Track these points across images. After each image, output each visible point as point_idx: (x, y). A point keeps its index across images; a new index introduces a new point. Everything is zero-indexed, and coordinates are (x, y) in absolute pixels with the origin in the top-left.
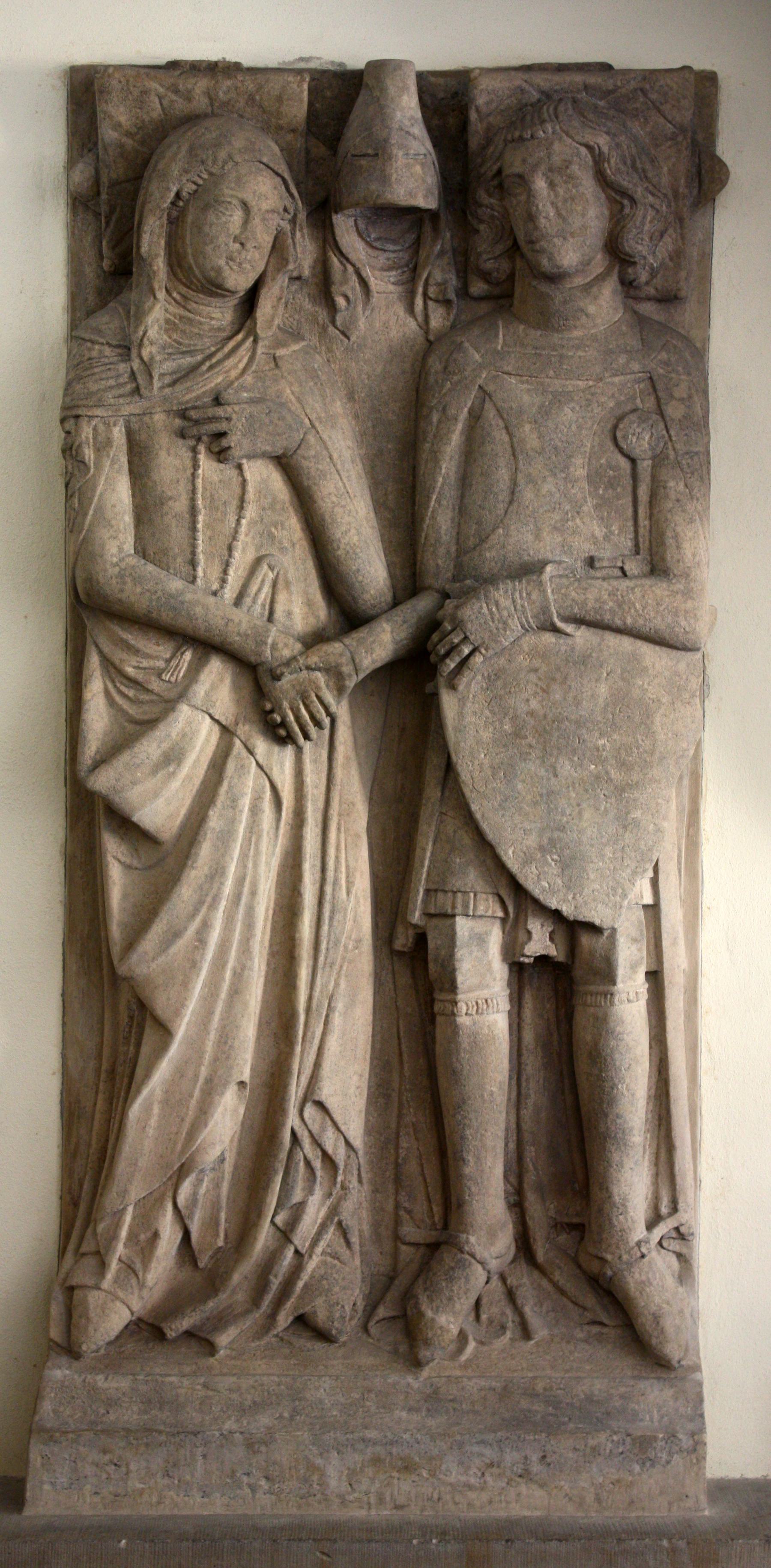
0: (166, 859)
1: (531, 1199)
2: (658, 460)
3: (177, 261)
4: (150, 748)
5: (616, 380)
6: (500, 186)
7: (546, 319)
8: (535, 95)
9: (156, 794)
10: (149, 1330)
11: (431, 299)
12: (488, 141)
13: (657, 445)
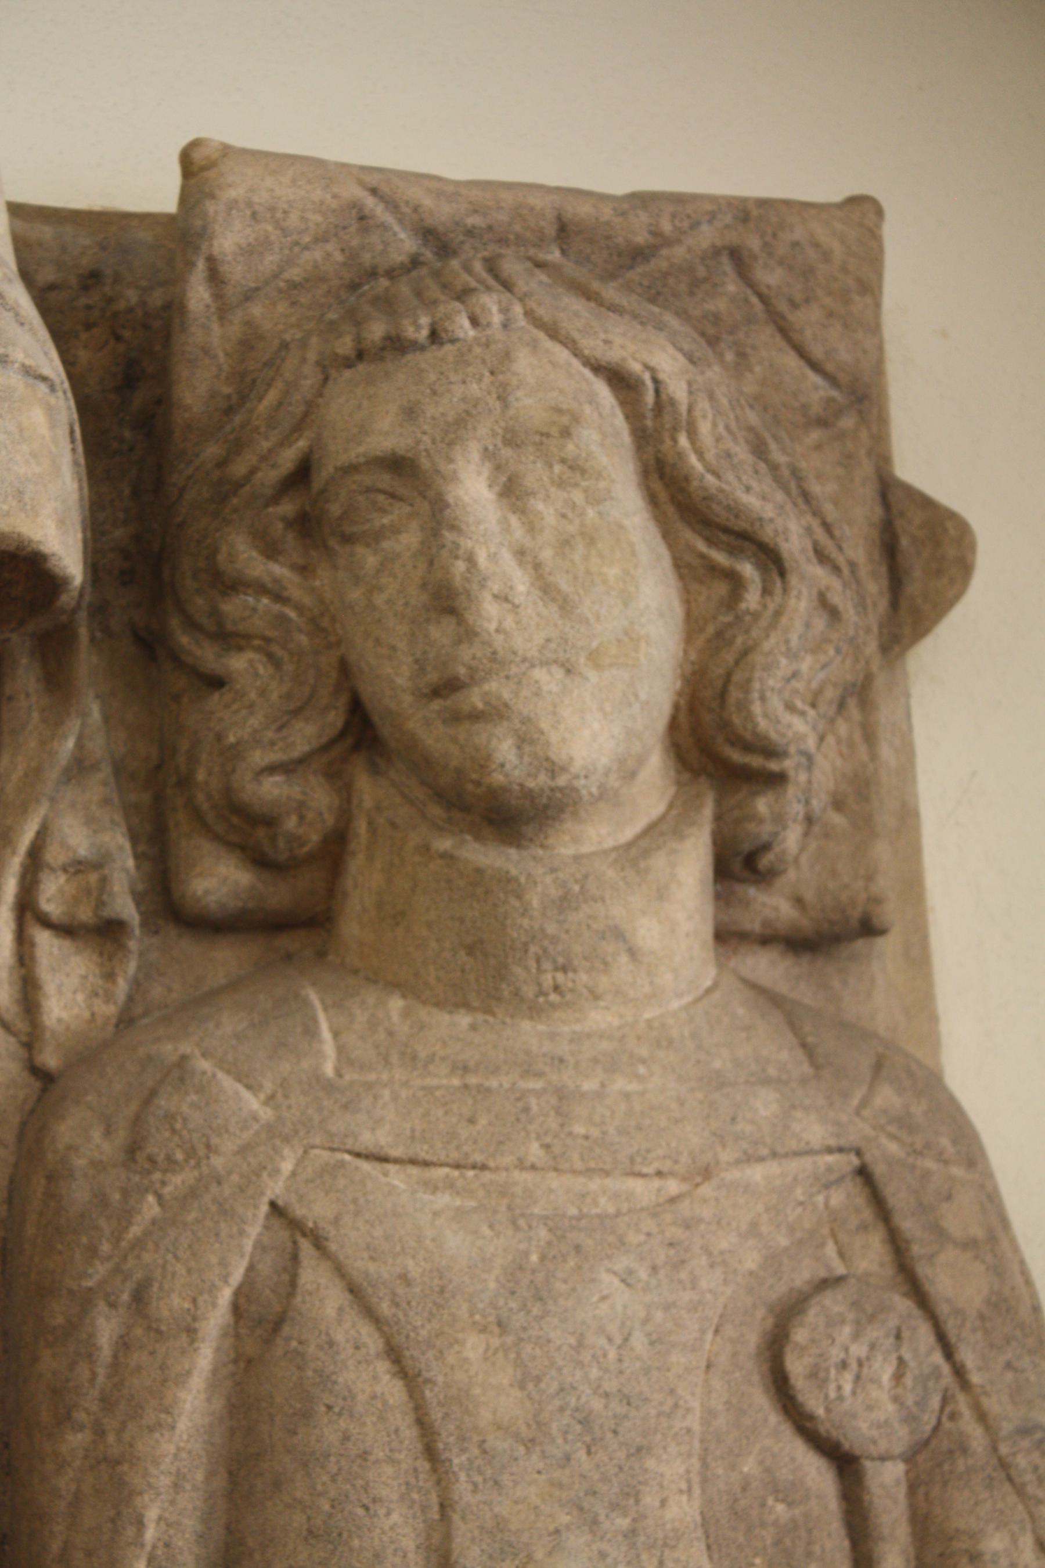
2: (931, 1460)
5: (757, 1174)
6: (308, 526)
7: (488, 967)
8: (405, 243)
11: (46, 922)
12: (245, 387)
13: (921, 1403)
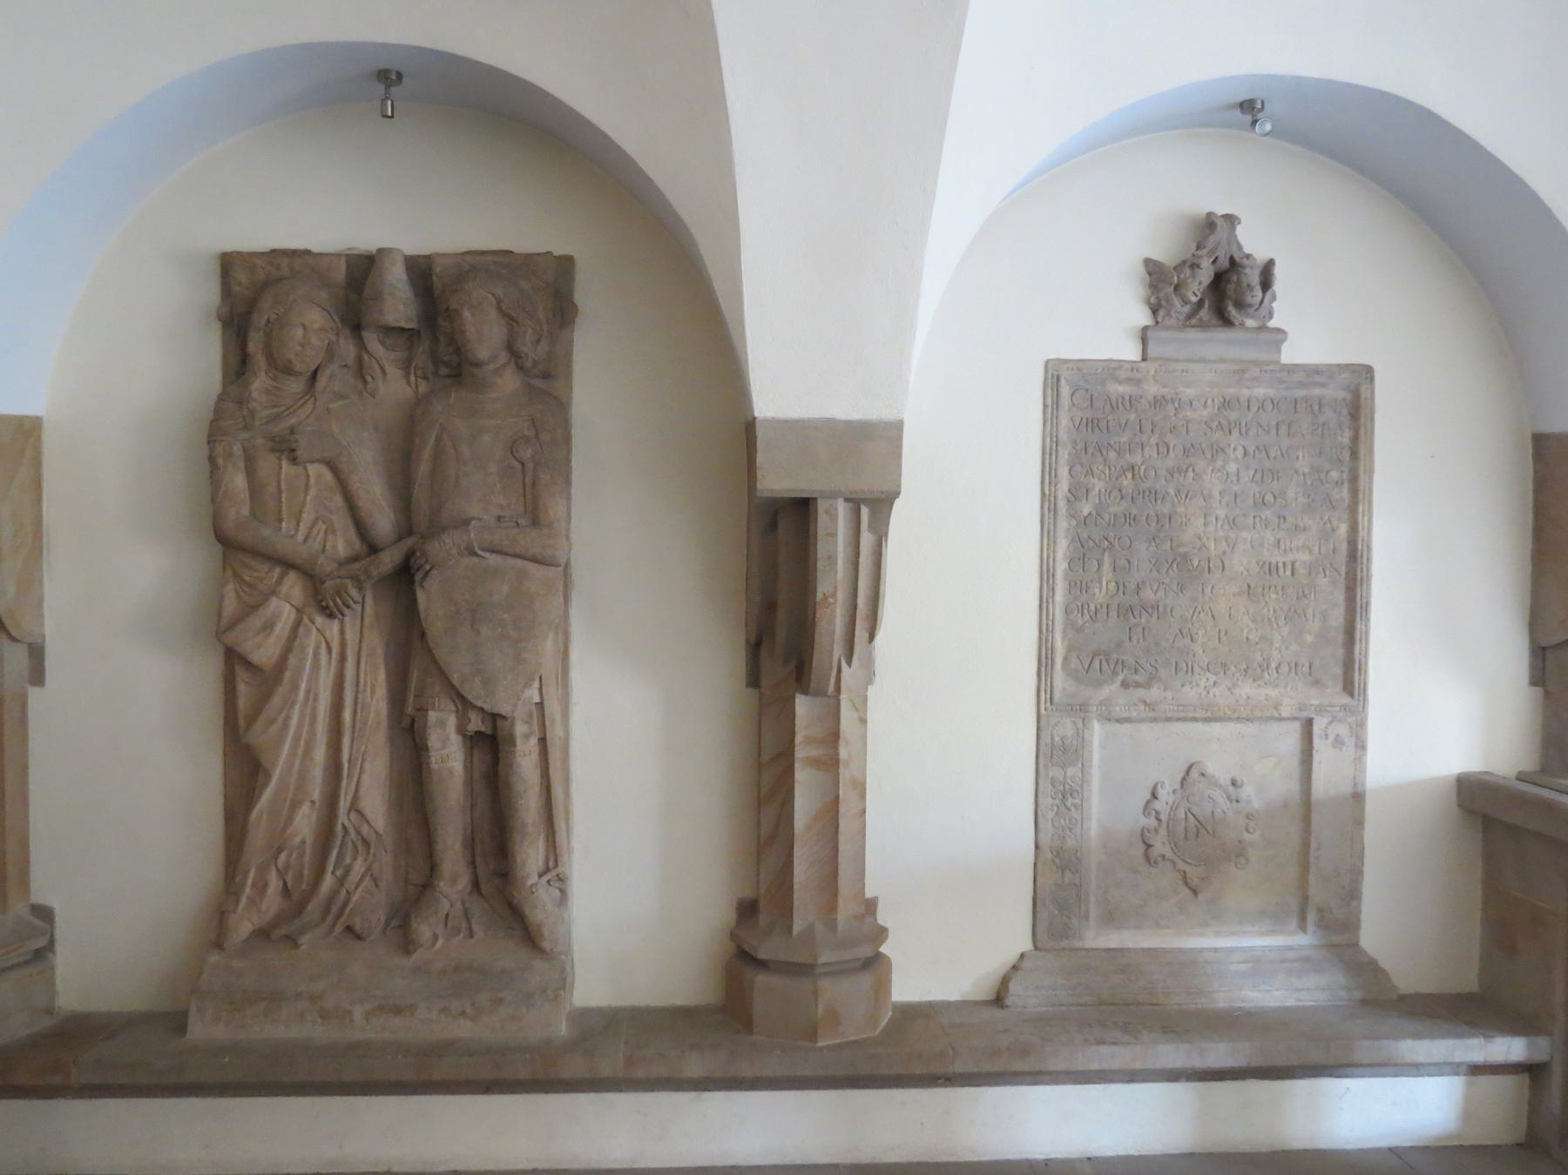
0: (270, 679)
1: (479, 860)
3: (270, 358)
4: (255, 621)
9: (259, 646)
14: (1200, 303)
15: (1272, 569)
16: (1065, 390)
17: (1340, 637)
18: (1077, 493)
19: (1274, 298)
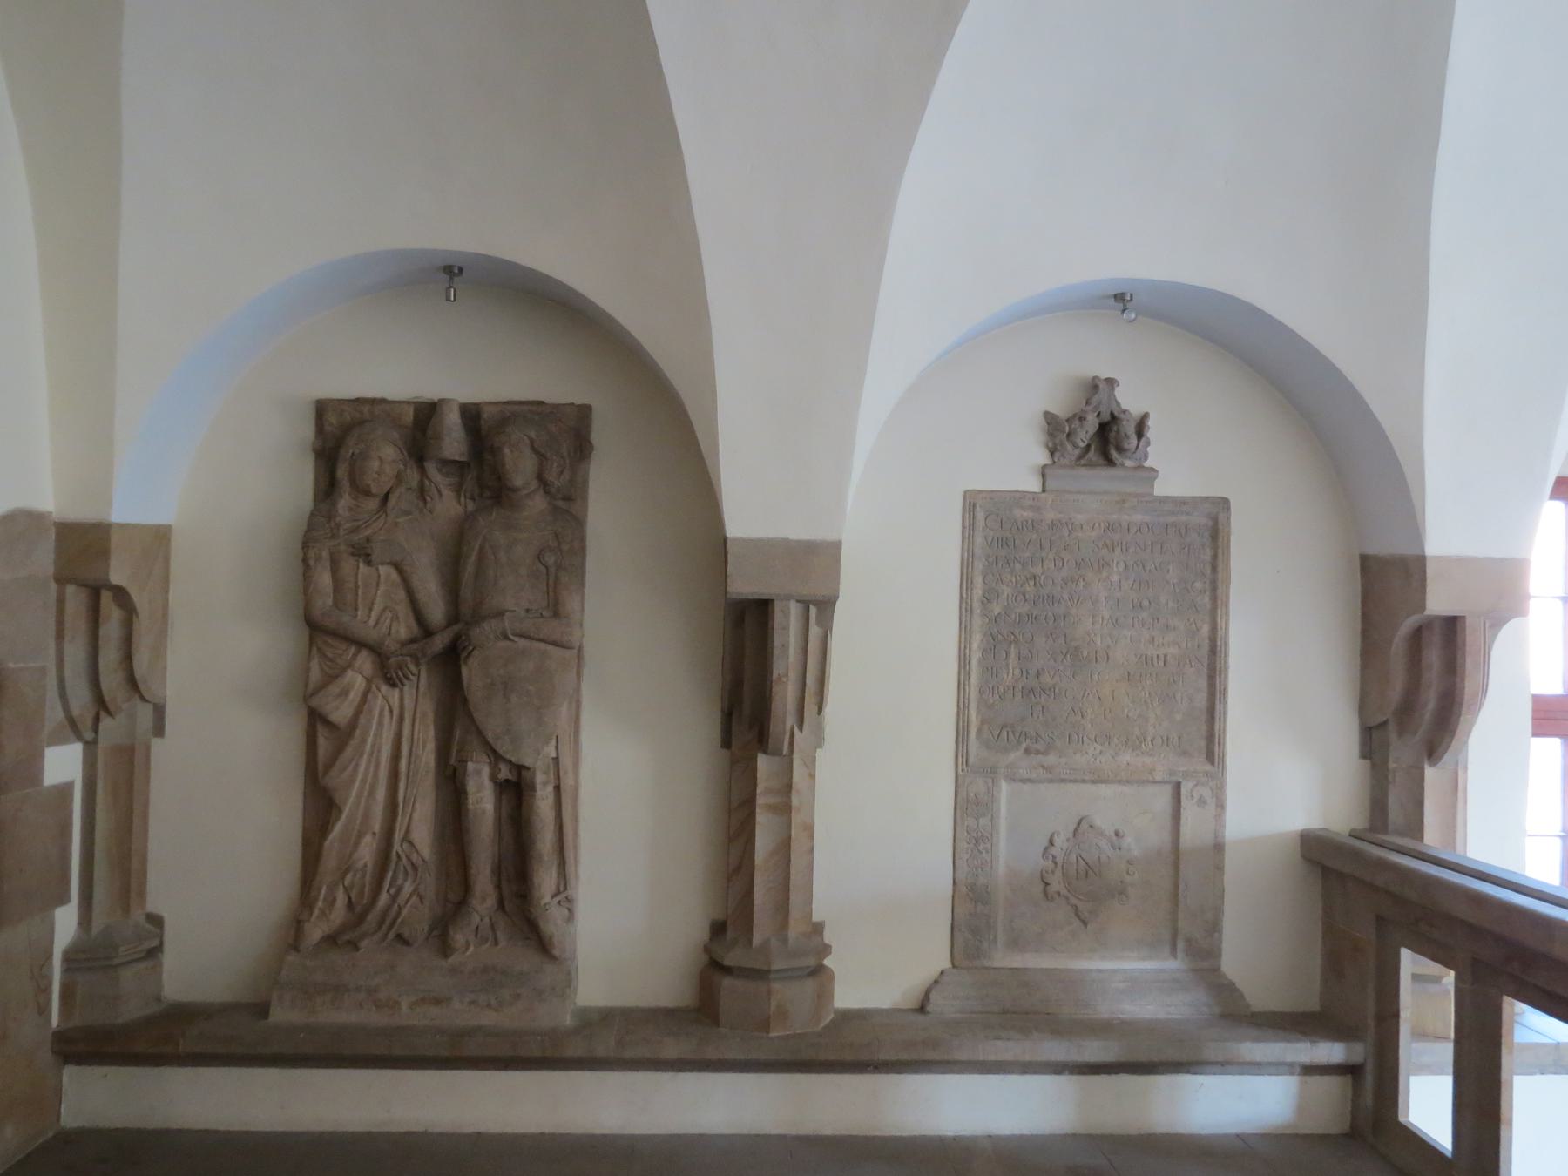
0: (344, 735)
1: (504, 885)
3: (353, 482)
4: (334, 689)
10: (331, 940)
14: (1088, 446)
15: (1147, 660)
16: (980, 515)
17: (1204, 717)
18: (989, 597)
19: (1148, 444)
